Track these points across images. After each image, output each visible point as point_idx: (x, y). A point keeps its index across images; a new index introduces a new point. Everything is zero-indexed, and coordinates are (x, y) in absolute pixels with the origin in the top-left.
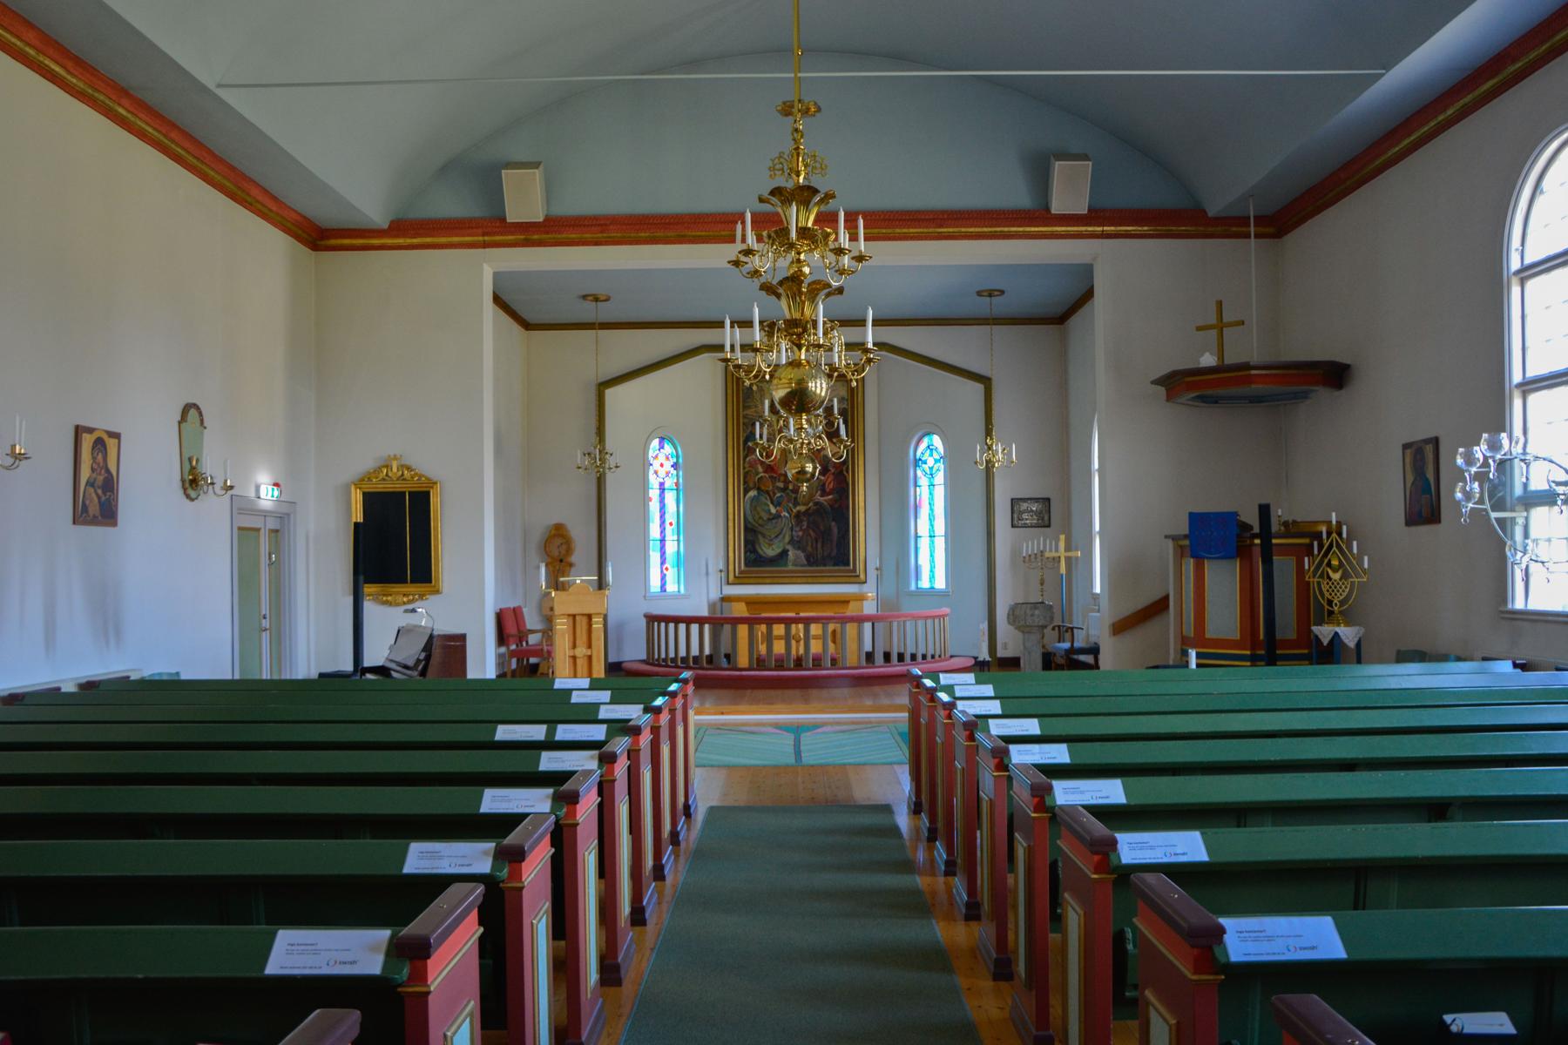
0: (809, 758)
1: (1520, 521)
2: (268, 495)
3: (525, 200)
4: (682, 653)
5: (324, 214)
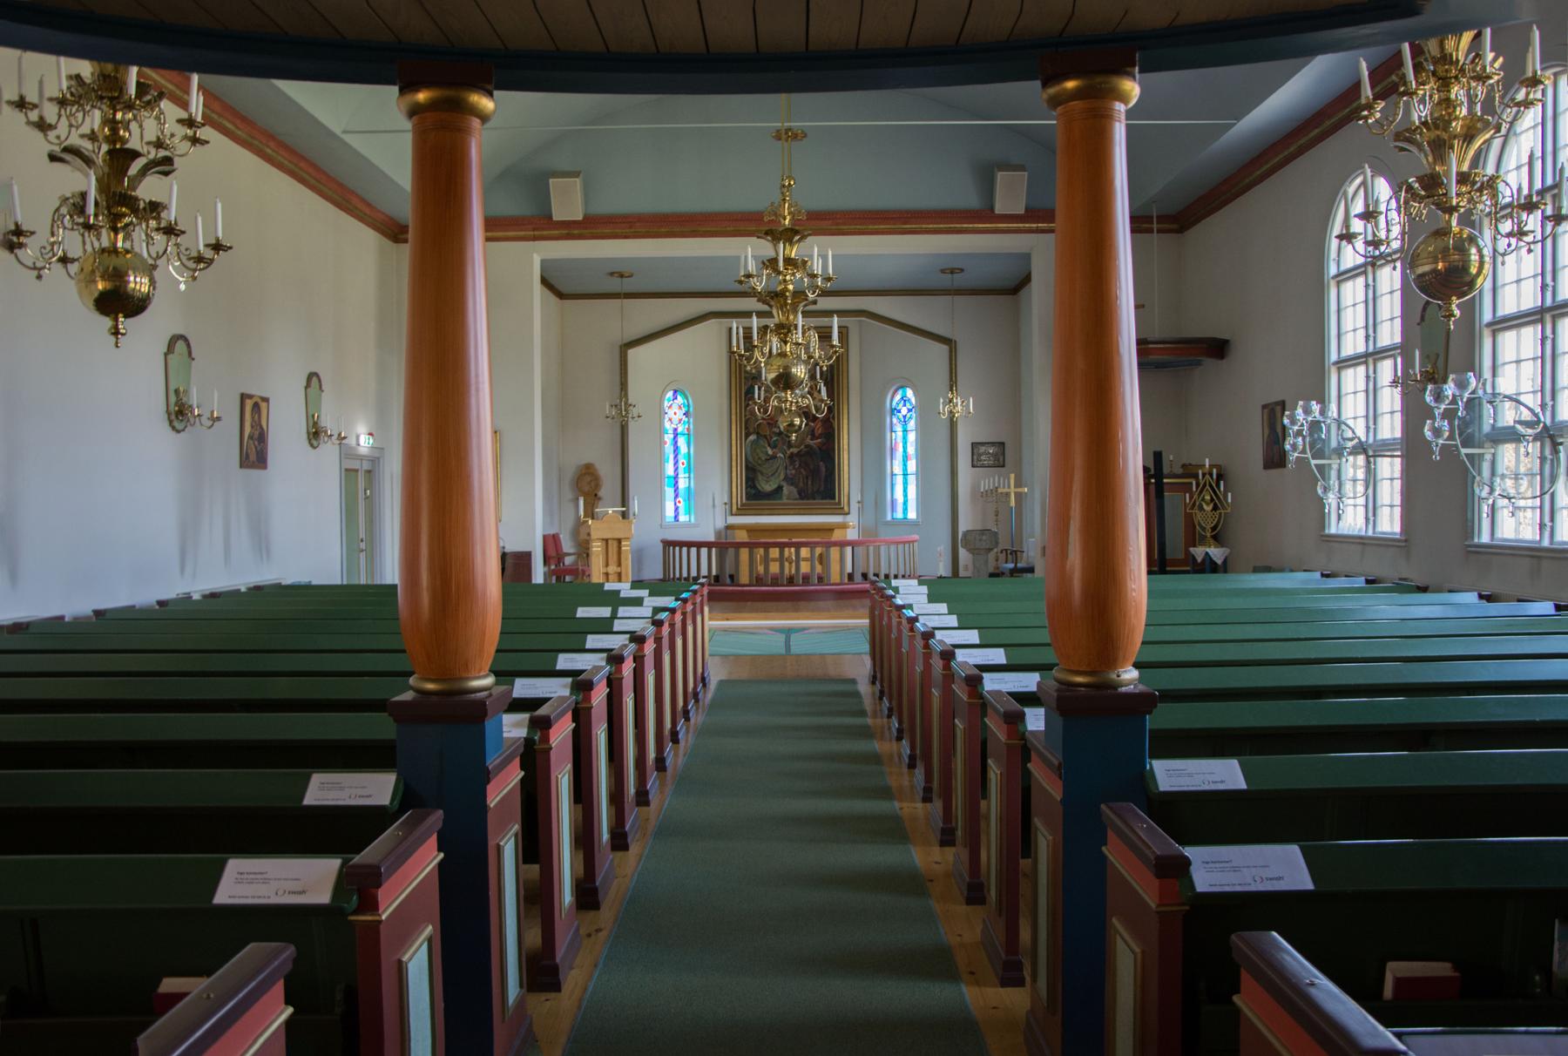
0: (795, 650)
2: (365, 442)
3: (568, 203)
4: (694, 573)
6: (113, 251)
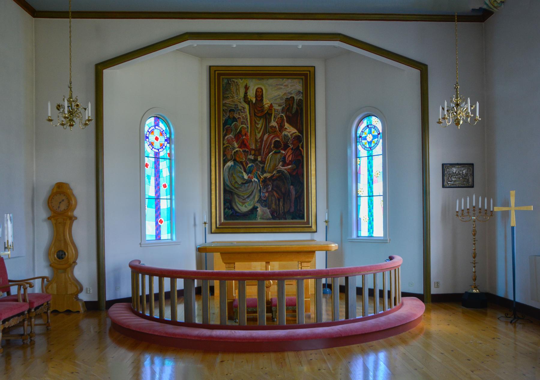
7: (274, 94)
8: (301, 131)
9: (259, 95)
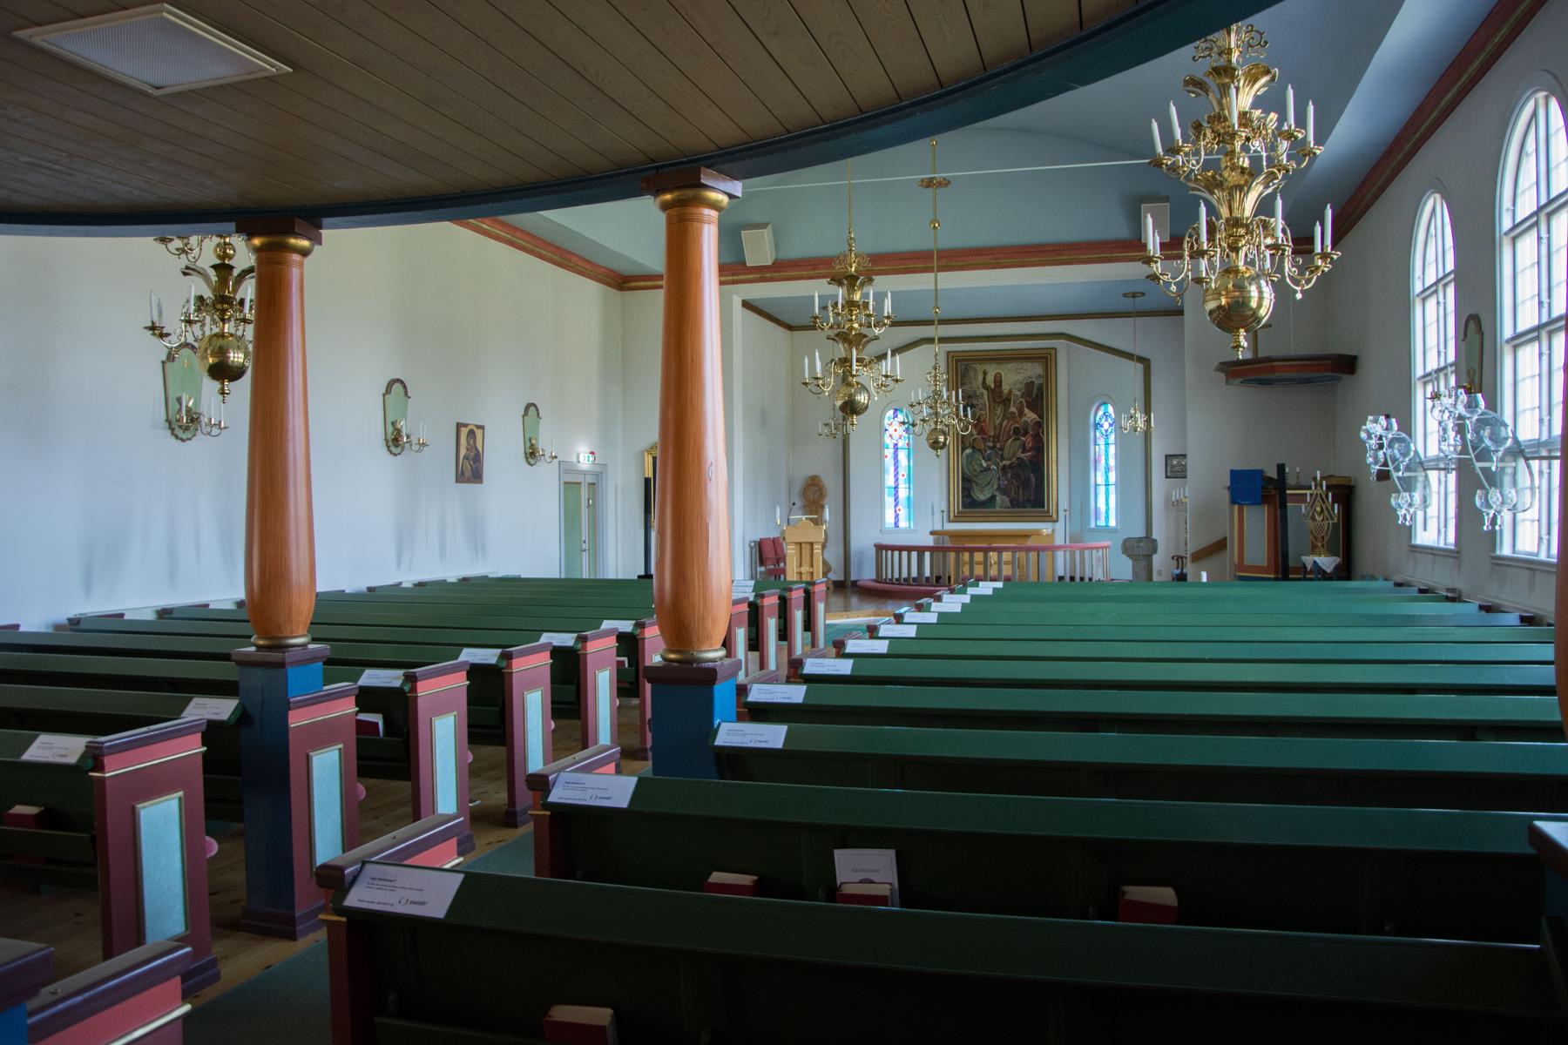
1: (1509, 471)
2: (585, 461)
4: (905, 575)
5: (626, 269)
6: (222, 335)
7: (1013, 378)
8: (1041, 417)
9: (998, 382)
